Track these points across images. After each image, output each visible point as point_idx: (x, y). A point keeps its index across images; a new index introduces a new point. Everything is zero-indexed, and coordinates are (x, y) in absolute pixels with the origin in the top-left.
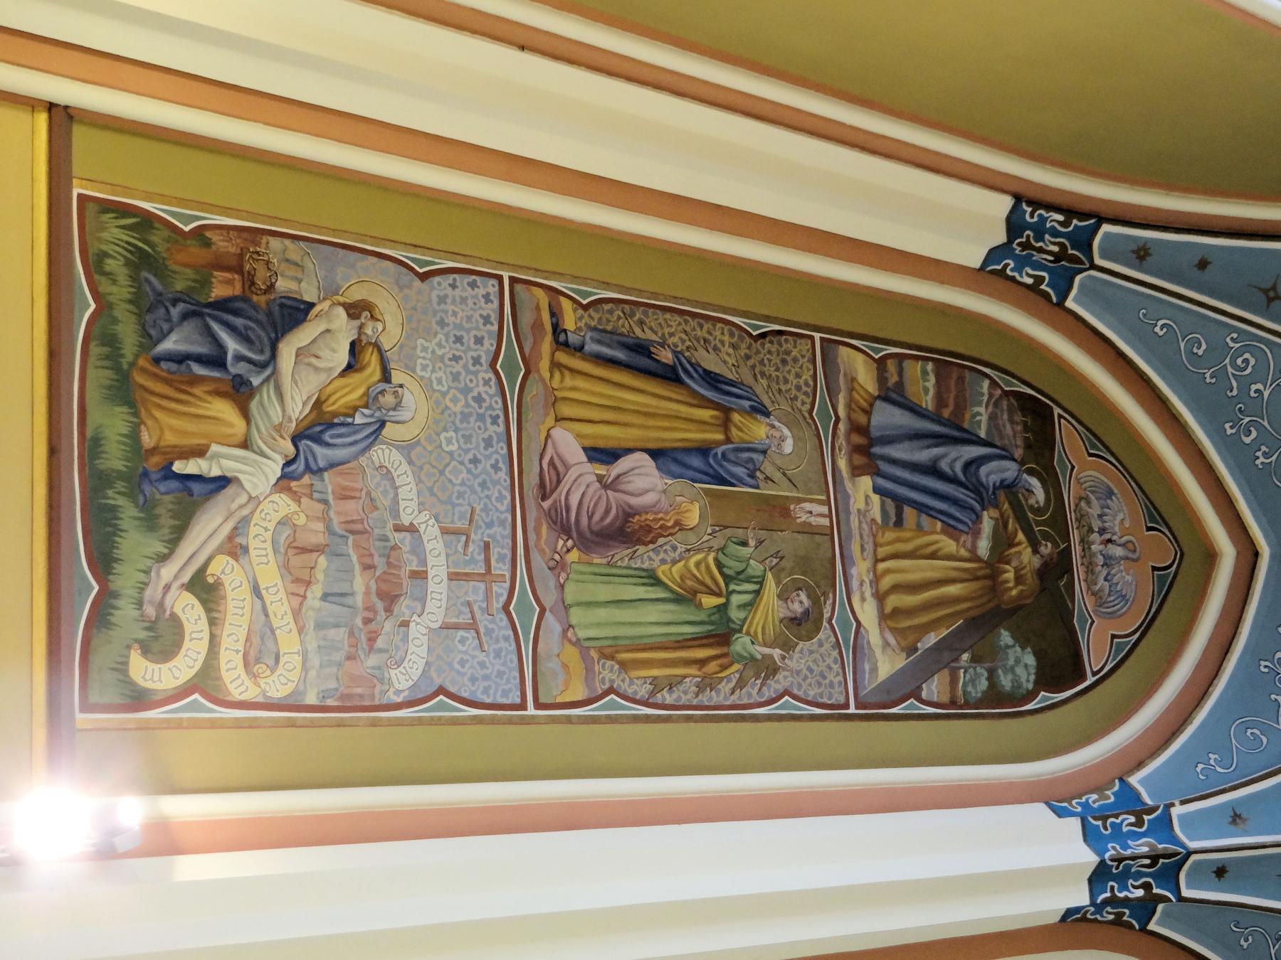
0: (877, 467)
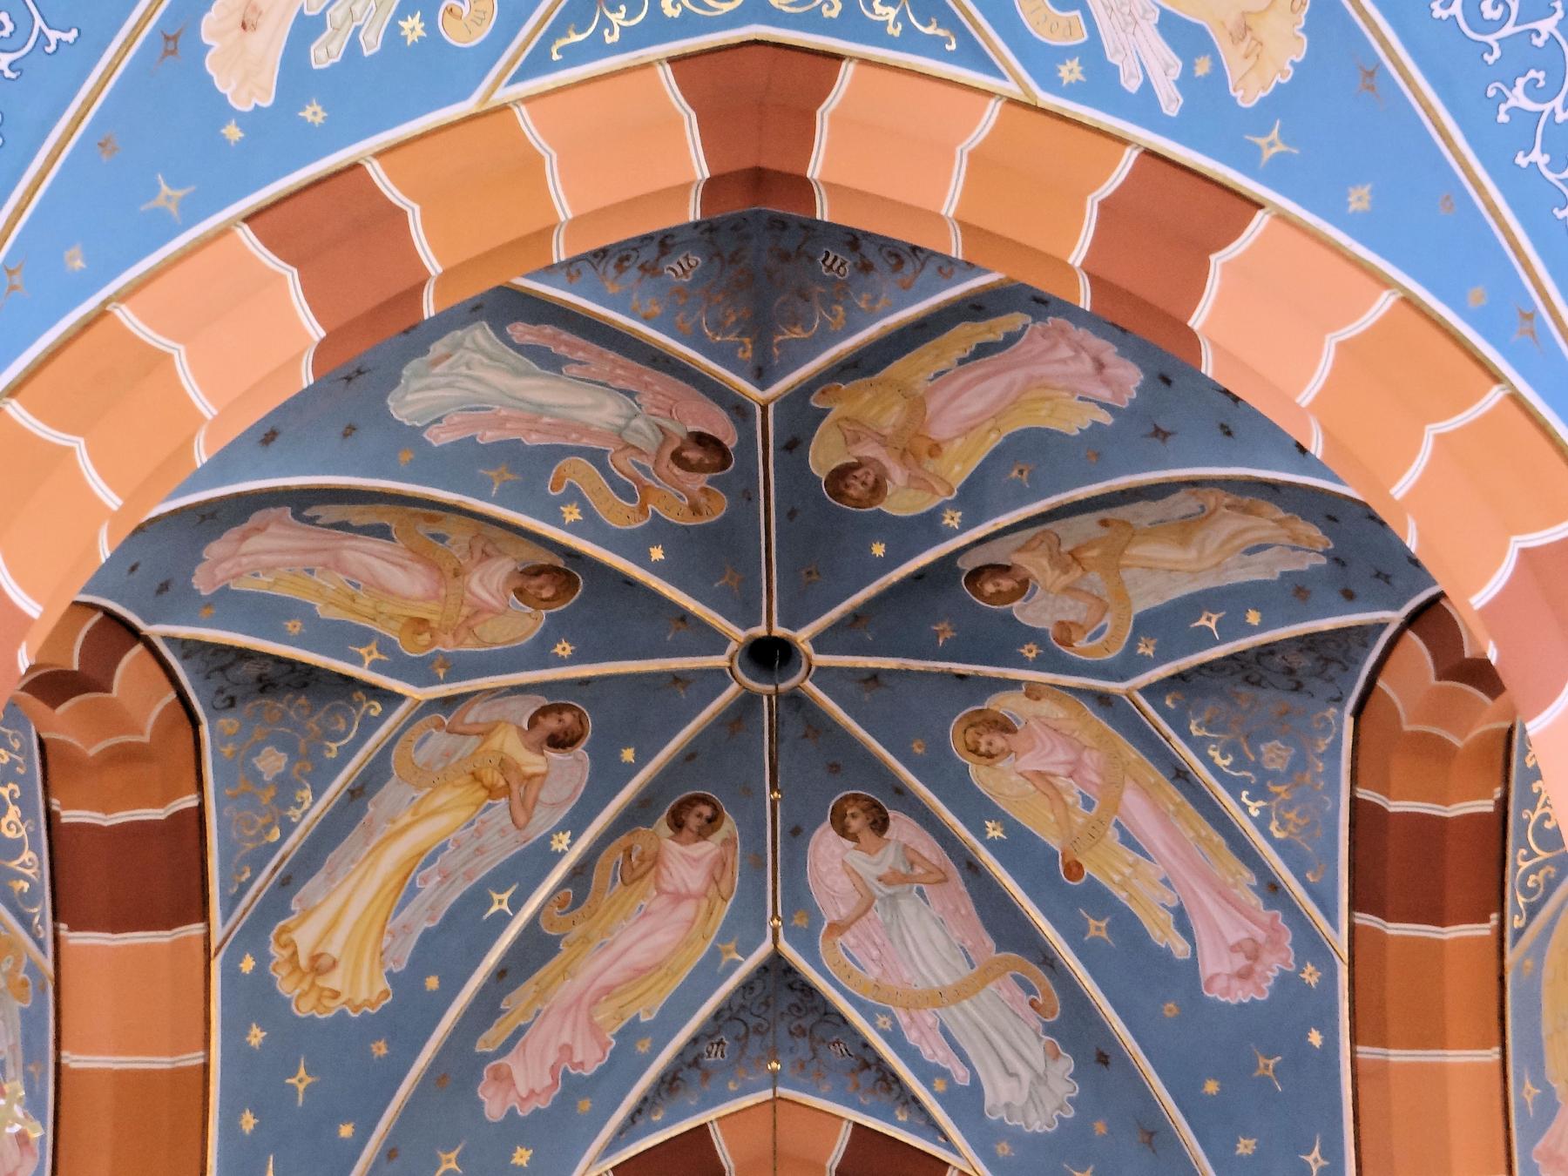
0: (515, 1128)
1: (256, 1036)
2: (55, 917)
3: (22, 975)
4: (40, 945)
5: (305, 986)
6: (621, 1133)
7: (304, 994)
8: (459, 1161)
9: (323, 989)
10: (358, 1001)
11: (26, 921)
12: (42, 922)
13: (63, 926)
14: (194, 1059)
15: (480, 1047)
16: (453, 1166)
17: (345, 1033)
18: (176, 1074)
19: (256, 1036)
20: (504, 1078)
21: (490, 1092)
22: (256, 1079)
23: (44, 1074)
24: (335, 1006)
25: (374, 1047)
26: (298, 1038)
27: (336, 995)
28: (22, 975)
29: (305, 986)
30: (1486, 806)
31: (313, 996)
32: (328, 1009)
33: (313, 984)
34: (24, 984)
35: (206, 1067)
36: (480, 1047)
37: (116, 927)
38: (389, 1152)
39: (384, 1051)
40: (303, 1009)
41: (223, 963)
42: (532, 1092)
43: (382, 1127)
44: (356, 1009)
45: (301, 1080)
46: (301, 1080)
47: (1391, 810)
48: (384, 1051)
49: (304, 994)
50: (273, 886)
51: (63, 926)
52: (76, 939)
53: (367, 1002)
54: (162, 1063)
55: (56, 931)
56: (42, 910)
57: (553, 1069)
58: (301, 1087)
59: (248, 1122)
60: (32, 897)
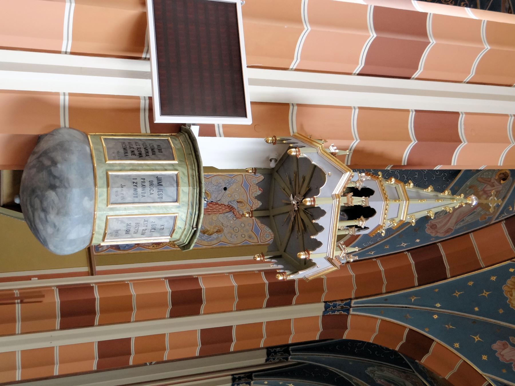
0: (492, 353)
1: (493, 278)
2: (505, 219)
3: (487, 217)
4: (497, 218)
5: (511, 287)
6: (500, 383)
7: (509, 287)
8: (478, 341)
9: (512, 292)
10: (512, 302)
11: (502, 213)
12: (503, 217)
13: (504, 222)
14: (482, 264)
15: (511, 338)
16: (476, 340)
17: (501, 300)
18: (477, 261)
19: (493, 278)
20: (504, 347)
21: (499, 344)
22: (483, 281)
23: (464, 231)
24: (509, 296)
25: (501, 310)
26: (496, 289)
27: (511, 295)
28: (487, 217)
29: (511, 287)
30: (409, 255)
31: (509, 290)
32: (507, 294)
33: (512, 289)
34: (485, 218)
35: (481, 268)
36: (511, 338)
37: (510, 234)
38: (475, 321)
39: (501, 312)
40: (505, 288)
41: (510, 263)
42: (503, 356)
43: (481, 318)
44: (510, 302)
45: (486, 294)
46: (486, 294)
47: (414, 262)
48: (501, 312)
49: (509, 287)
50: (120, 238)
51: (504, 222)
52: (503, 225)
53: (512, 304)
54: (479, 257)
55: (502, 220)
56: (506, 215)
57: (511, 360)
58: (484, 294)
59: (471, 283)
60: (508, 212)
